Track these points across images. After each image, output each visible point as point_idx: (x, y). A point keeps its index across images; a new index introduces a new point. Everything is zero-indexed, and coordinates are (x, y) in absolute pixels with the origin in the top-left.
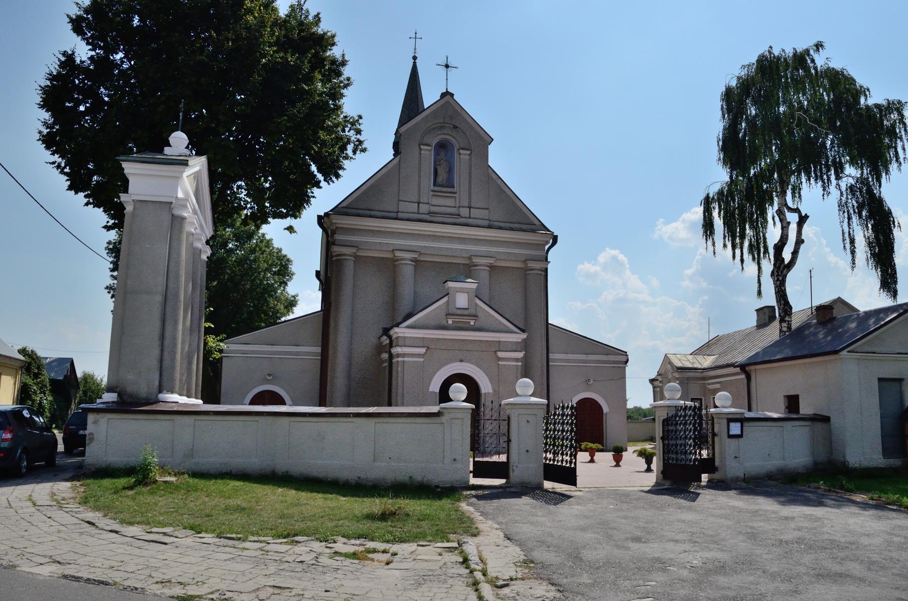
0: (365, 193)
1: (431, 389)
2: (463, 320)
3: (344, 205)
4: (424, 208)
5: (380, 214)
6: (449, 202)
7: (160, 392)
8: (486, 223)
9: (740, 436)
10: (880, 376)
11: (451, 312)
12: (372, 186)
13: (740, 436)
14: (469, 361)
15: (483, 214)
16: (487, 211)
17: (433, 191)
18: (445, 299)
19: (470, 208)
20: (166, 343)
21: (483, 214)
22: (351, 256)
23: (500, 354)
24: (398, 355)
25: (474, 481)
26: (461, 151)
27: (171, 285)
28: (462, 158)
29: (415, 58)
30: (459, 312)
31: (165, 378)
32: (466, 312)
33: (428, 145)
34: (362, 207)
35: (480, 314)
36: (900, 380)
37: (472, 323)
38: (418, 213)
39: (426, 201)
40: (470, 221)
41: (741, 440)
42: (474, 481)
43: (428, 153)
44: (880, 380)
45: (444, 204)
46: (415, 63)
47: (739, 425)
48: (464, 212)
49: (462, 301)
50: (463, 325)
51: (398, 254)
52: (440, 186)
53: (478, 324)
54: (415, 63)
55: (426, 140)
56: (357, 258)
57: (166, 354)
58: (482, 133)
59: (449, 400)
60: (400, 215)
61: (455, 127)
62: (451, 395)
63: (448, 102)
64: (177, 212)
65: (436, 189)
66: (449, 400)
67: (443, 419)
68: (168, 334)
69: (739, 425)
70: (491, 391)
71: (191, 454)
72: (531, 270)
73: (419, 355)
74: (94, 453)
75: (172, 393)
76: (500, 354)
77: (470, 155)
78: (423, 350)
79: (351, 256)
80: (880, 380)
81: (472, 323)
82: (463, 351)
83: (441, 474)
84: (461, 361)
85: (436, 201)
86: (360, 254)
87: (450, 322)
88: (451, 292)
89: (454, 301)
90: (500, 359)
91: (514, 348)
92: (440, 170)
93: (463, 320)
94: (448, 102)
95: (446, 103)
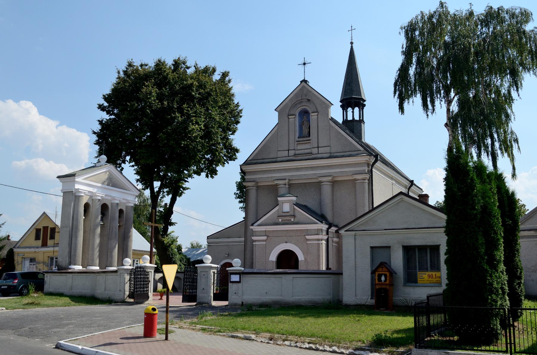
0: (261, 150)
1: (270, 259)
2: (287, 219)
3: (250, 159)
4: (292, 153)
5: (269, 160)
6: (307, 146)
7: (70, 265)
8: (328, 155)
9: (239, 282)
10: (372, 245)
11: (280, 215)
12: (264, 146)
13: (239, 282)
14: (291, 242)
15: (327, 150)
18: (277, 208)
19: (318, 147)
20: (73, 245)
22: (253, 186)
23: (307, 237)
24: (255, 241)
25: (214, 303)
26: (312, 114)
27: (74, 223)
28: (313, 117)
29: (352, 43)
30: (284, 214)
31: (72, 259)
32: (288, 214)
33: (293, 115)
34: (260, 158)
35: (297, 214)
36: (389, 247)
37: (292, 220)
38: (288, 156)
39: (293, 148)
40: (319, 156)
41: (240, 285)
42: (214, 303)
43: (293, 119)
44: (372, 248)
45: (303, 148)
46: (352, 47)
47: (238, 276)
48: (315, 151)
49: (286, 208)
50: (286, 221)
51: (276, 182)
52: (304, 137)
53: (296, 220)
54: (352, 47)
55: (293, 112)
56: (258, 187)
57: (72, 250)
58: (324, 100)
59: (123, 265)
60: (279, 159)
61: (309, 100)
62: (124, 264)
63: (304, 86)
64: (76, 194)
65: (300, 139)
66: (123, 265)
67: (118, 273)
68: (73, 242)
69: (238, 276)
70: (303, 259)
71: (71, 288)
72: (357, 180)
73: (263, 241)
74: (47, 288)
75: (75, 265)
76: (307, 237)
77: (317, 115)
78: (265, 238)
79: (253, 186)
80: (372, 248)
81: (292, 220)
82: (287, 236)
83: (118, 297)
84: (286, 242)
85: (299, 147)
86: (260, 184)
87: (280, 220)
88: (279, 203)
89: (282, 208)
90: (308, 240)
91: (316, 232)
93: (287, 219)
94: (304, 86)
95: (302, 87)
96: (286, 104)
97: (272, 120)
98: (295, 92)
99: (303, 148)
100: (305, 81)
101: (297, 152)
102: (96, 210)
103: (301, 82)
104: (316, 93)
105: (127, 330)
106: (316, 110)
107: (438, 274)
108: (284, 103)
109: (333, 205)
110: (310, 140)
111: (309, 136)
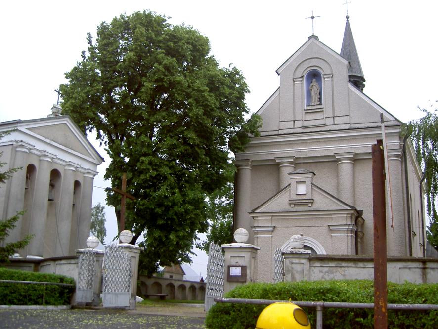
4: (298, 124)
8: (347, 127)
15: (345, 120)
16: (348, 117)
17: (306, 110)
21: (345, 120)
26: (325, 76)
48: (329, 121)
60: (281, 132)
63: (103, 160)
65: (308, 108)
92: (313, 93)
96: (291, 64)
97: (275, 82)
98: (302, 49)
99: (315, 120)
100: (314, 37)
101: (306, 124)
102: (43, 177)
103: (310, 38)
104: (329, 51)
105: (411, 306)
106: (330, 73)
107: (319, 308)
108: (288, 63)
109: (354, 191)
110: (290, 200)
111: (321, 104)
